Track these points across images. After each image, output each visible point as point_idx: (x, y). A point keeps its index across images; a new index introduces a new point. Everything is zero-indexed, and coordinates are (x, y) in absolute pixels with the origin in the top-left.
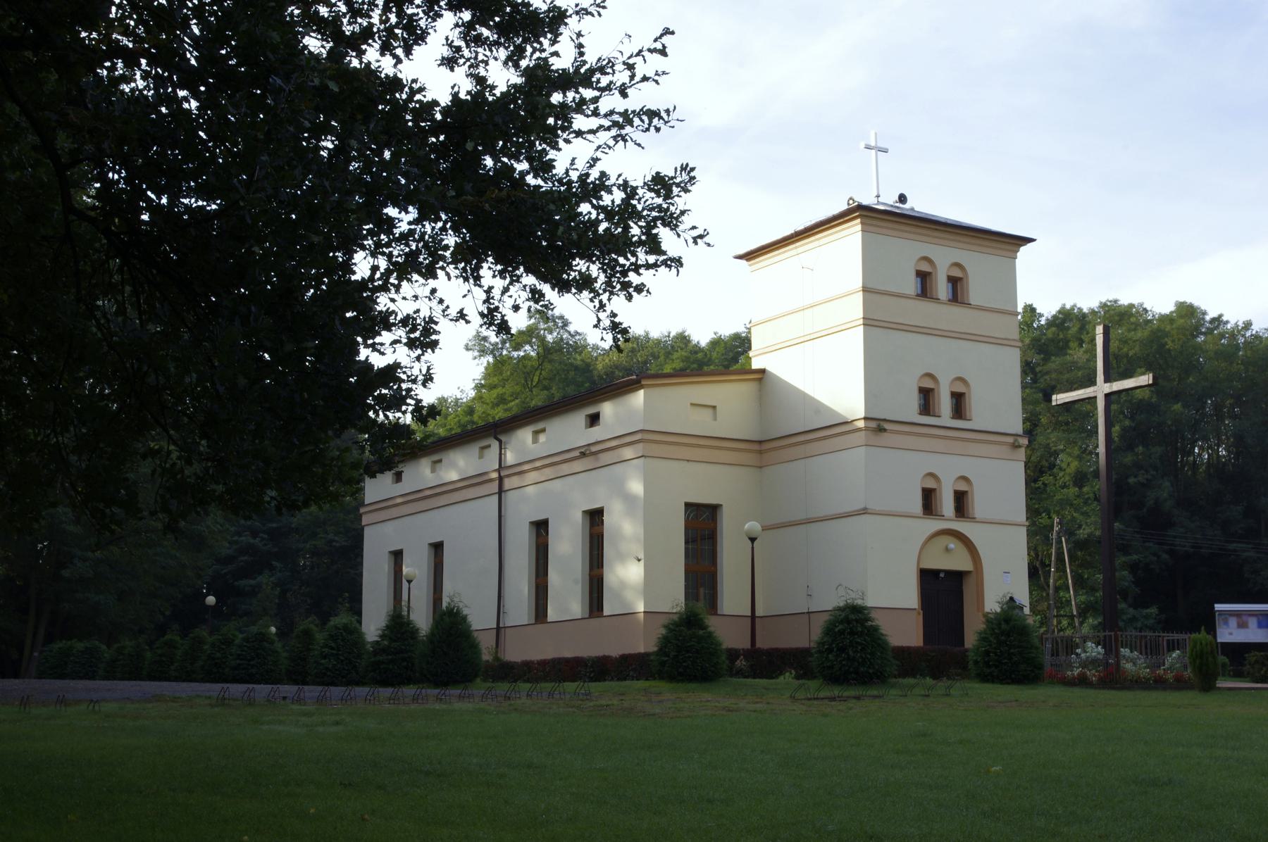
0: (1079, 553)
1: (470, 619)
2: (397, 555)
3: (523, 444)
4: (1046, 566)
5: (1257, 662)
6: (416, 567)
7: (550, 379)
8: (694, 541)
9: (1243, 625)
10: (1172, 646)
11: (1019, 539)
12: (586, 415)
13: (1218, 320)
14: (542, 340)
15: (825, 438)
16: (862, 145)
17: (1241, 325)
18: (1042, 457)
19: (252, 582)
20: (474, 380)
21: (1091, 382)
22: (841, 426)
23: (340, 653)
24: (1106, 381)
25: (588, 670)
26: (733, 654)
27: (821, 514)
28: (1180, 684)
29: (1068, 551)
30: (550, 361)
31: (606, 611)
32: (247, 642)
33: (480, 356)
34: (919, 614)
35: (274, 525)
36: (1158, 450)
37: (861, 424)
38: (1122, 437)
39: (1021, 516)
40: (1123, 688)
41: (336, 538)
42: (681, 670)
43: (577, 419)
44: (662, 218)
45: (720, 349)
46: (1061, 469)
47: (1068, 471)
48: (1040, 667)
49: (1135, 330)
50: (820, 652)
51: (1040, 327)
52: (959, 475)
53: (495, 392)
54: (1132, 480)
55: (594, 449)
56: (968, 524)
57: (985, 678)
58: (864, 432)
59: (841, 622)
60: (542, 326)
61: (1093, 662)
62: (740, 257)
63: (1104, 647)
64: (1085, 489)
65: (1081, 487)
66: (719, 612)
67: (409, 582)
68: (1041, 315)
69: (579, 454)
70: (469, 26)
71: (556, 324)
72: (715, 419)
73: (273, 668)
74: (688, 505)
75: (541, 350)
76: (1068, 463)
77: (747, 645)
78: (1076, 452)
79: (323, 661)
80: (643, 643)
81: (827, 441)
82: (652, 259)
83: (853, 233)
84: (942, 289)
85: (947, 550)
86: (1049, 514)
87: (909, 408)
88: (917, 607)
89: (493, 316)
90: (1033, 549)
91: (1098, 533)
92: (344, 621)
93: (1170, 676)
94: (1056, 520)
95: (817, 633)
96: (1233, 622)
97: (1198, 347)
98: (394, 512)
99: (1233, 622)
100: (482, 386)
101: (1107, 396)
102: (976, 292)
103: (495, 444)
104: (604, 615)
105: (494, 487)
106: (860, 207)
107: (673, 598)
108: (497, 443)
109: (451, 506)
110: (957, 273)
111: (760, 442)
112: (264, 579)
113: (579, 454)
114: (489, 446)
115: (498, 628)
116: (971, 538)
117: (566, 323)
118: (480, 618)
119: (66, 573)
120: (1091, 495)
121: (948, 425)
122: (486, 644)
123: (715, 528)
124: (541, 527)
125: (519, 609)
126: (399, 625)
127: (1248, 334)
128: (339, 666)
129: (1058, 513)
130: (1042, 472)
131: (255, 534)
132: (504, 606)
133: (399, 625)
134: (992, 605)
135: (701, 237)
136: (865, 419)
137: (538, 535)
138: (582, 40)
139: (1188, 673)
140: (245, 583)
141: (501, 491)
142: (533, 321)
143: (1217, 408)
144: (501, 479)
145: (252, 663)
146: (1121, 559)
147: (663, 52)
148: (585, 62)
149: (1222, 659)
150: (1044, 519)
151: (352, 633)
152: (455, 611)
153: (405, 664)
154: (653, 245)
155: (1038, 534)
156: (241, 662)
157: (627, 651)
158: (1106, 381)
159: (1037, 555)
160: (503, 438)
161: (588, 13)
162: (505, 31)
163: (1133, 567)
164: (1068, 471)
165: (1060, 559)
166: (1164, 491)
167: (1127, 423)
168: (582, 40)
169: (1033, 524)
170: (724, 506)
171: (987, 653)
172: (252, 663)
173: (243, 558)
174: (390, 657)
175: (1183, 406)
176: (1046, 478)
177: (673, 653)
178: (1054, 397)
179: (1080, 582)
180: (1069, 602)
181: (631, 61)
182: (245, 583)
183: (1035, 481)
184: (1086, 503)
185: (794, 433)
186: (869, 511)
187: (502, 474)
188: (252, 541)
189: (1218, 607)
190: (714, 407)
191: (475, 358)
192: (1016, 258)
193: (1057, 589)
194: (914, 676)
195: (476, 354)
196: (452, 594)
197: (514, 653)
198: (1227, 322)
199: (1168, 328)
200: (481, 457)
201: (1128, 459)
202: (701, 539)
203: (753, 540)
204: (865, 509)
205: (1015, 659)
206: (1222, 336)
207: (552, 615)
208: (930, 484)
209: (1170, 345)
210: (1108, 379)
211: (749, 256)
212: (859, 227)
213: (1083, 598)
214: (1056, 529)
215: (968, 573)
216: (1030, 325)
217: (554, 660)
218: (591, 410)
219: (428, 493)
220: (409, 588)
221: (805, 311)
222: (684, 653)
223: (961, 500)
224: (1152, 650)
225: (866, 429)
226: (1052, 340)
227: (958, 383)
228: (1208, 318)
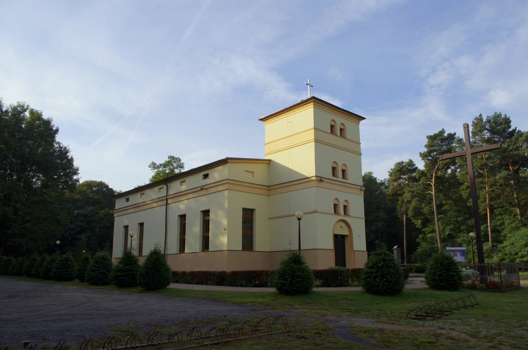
2: (126, 227)
6: (134, 231)
11: (363, 223)
12: (203, 175)
15: (275, 189)
16: (305, 83)
19: (80, 236)
20: (150, 179)
22: (305, 180)
23: (100, 269)
25: (215, 278)
32: (61, 262)
33: (153, 169)
34: (334, 251)
35: (88, 219)
37: (314, 178)
39: (363, 215)
41: (107, 224)
42: (294, 288)
55: (206, 187)
56: (347, 217)
58: (315, 181)
66: (254, 250)
67: (132, 237)
69: (200, 189)
72: (253, 177)
73: (71, 272)
79: (92, 273)
81: (290, 187)
85: (341, 227)
87: (329, 175)
88: (333, 248)
98: (127, 212)
102: (348, 133)
104: (209, 251)
105: (165, 202)
108: (166, 186)
109: (144, 211)
111: (269, 186)
113: (200, 189)
114: (163, 188)
116: (347, 221)
117: (180, 160)
121: (341, 181)
124: (183, 217)
125: (173, 247)
128: (99, 276)
132: (167, 246)
136: (316, 176)
137: (181, 220)
142: (170, 159)
144: (167, 200)
145: (62, 271)
151: (105, 262)
152: (158, 252)
153: (131, 277)
156: (57, 270)
160: (168, 184)
172: (62, 271)
173: (78, 229)
174: (124, 273)
177: (290, 279)
185: (274, 184)
186: (317, 212)
187: (167, 198)
188: (81, 224)
190: (253, 172)
191: (152, 170)
195: (152, 168)
196: (157, 243)
200: (159, 192)
202: (248, 222)
204: (316, 211)
212: (312, 106)
215: (347, 236)
219: (141, 204)
220: (131, 240)
221: (289, 138)
222: (295, 278)
227: (344, 166)
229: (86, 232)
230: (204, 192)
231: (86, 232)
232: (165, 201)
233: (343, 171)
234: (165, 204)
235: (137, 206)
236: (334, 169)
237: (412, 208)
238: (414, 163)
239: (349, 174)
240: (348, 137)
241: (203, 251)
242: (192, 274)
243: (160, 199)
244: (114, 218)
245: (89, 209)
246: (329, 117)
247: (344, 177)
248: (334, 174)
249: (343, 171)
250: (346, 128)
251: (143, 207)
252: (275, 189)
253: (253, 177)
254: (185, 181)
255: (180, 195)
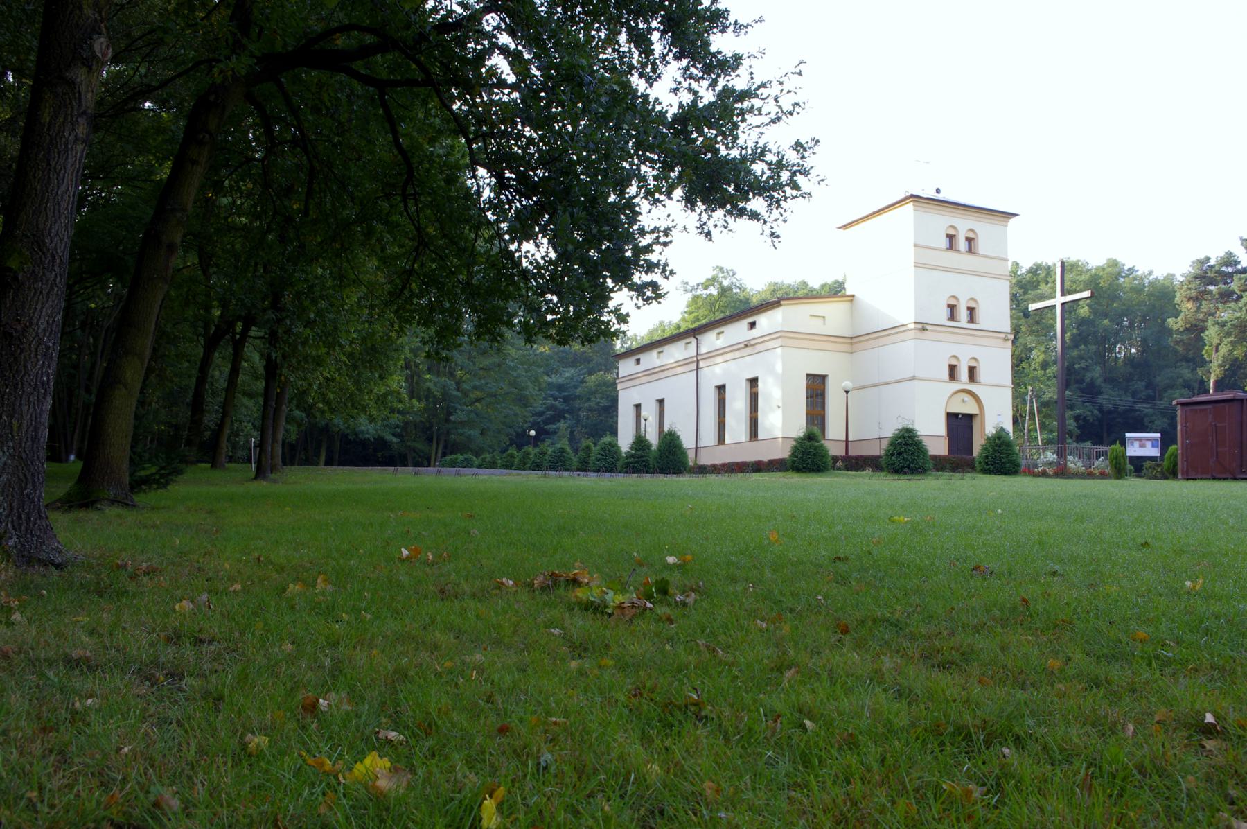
0: (1044, 410)
1: (681, 437)
2: (638, 407)
3: (710, 341)
4: (1023, 417)
5: (1150, 467)
6: (650, 413)
7: (726, 307)
8: (811, 397)
9: (1142, 446)
10: (1098, 455)
11: (1007, 394)
13: (1132, 270)
14: (721, 283)
17: (1147, 273)
18: (1022, 351)
19: (554, 426)
21: (1052, 296)
22: (895, 330)
24: (1062, 295)
26: (835, 459)
27: (888, 380)
28: (1103, 475)
29: (1037, 408)
30: (726, 296)
31: (760, 437)
36: (1093, 348)
37: (912, 326)
38: (1071, 340)
40: (1068, 478)
43: (744, 323)
44: (799, 171)
45: (827, 289)
46: (1033, 359)
47: (1038, 360)
48: (1018, 465)
49: (1081, 275)
50: (887, 455)
51: (1022, 275)
52: (972, 356)
53: (693, 316)
54: (1077, 366)
55: (752, 342)
57: (986, 471)
59: (900, 438)
60: (721, 275)
61: (1051, 463)
62: (840, 228)
63: (1057, 455)
64: (1048, 371)
65: (1045, 370)
67: (645, 420)
68: (1022, 267)
70: (687, 69)
71: (728, 274)
72: (824, 324)
74: (808, 375)
75: (720, 290)
76: (1037, 355)
77: (843, 454)
78: (1043, 348)
80: (782, 452)
82: (795, 193)
83: (909, 207)
84: (962, 245)
85: (963, 401)
86: (1025, 386)
87: (942, 316)
89: (703, 229)
90: (1015, 407)
91: (1055, 397)
92: (609, 440)
93: (1097, 471)
94: (1030, 388)
95: (885, 444)
96: (1137, 444)
97: (1119, 285)
98: (637, 382)
99: (1137, 444)
100: (685, 312)
101: (1063, 304)
102: (982, 246)
103: (694, 341)
105: (694, 366)
106: (912, 196)
107: (798, 427)
108: (695, 340)
110: (971, 235)
111: (851, 338)
112: (562, 425)
114: (690, 342)
115: (697, 448)
118: (688, 442)
119: (452, 418)
120: (1052, 375)
122: (691, 455)
123: (824, 389)
124: (721, 389)
126: (640, 443)
127: (1151, 278)
129: (1031, 385)
130: (1021, 361)
131: (555, 399)
133: (640, 443)
134: (990, 430)
135: (822, 180)
137: (751, 387)
138: (752, 70)
139: (1108, 470)
140: (551, 427)
141: (697, 369)
143: (1131, 325)
144: (698, 361)
146: (1069, 413)
147: (800, 74)
148: (754, 83)
149: (1129, 467)
150: (1022, 390)
151: (613, 449)
154: (795, 186)
155: (1018, 397)
157: (772, 458)
158: (1062, 295)
159: (1018, 410)
160: (698, 337)
161: (755, 57)
162: (708, 69)
163: (1077, 418)
164: (1038, 360)
165: (1032, 414)
166: (1096, 373)
167: (1075, 331)
168: (752, 70)
169: (1016, 391)
170: (830, 377)
171: (987, 457)
175: (1110, 321)
176: (1024, 365)
177: (800, 456)
178: (1030, 306)
179: (1043, 427)
180: (1037, 438)
181: (781, 80)
182: (551, 427)
183: (1018, 366)
184: (1048, 380)
189: (1128, 435)
190: (824, 317)
192: (1007, 226)
193: (1029, 431)
194: (943, 471)
197: (705, 460)
198: (1137, 271)
199: (1101, 273)
200: (686, 349)
201: (1075, 353)
203: (847, 392)
205: (1003, 460)
206: (1135, 279)
207: (727, 440)
208: (954, 362)
209: (1102, 284)
210: (1063, 294)
211: (845, 227)
213: (1045, 436)
214: (1030, 393)
215: (976, 415)
216: (1015, 273)
217: (729, 463)
218: (751, 320)
219: (657, 370)
223: (972, 370)
224: (1088, 457)
225: (916, 329)
226: (1029, 282)
228: (1126, 268)
229: (565, 418)
230: (748, 351)
231: (565, 418)
232: (695, 364)
233: (971, 310)
234: (695, 368)
235: (651, 372)
236: (952, 308)
237: (1220, 359)
238: (1239, 260)
239: (981, 314)
240: (981, 252)
241: (751, 440)
242: (724, 465)
243: (686, 362)
244: (617, 391)
245: (567, 374)
246: (941, 222)
247: (972, 319)
248: (952, 317)
249: (971, 310)
250: (979, 237)
251: (660, 374)
252: (866, 341)
253: (824, 324)
254: (723, 332)
255: (712, 355)
